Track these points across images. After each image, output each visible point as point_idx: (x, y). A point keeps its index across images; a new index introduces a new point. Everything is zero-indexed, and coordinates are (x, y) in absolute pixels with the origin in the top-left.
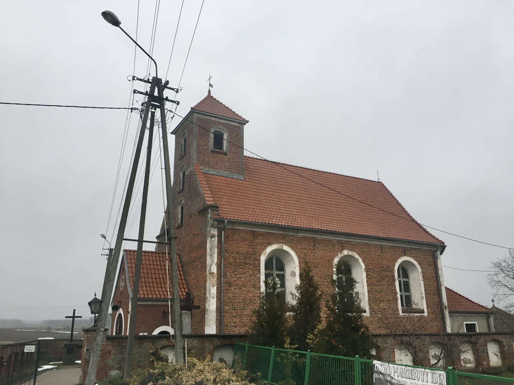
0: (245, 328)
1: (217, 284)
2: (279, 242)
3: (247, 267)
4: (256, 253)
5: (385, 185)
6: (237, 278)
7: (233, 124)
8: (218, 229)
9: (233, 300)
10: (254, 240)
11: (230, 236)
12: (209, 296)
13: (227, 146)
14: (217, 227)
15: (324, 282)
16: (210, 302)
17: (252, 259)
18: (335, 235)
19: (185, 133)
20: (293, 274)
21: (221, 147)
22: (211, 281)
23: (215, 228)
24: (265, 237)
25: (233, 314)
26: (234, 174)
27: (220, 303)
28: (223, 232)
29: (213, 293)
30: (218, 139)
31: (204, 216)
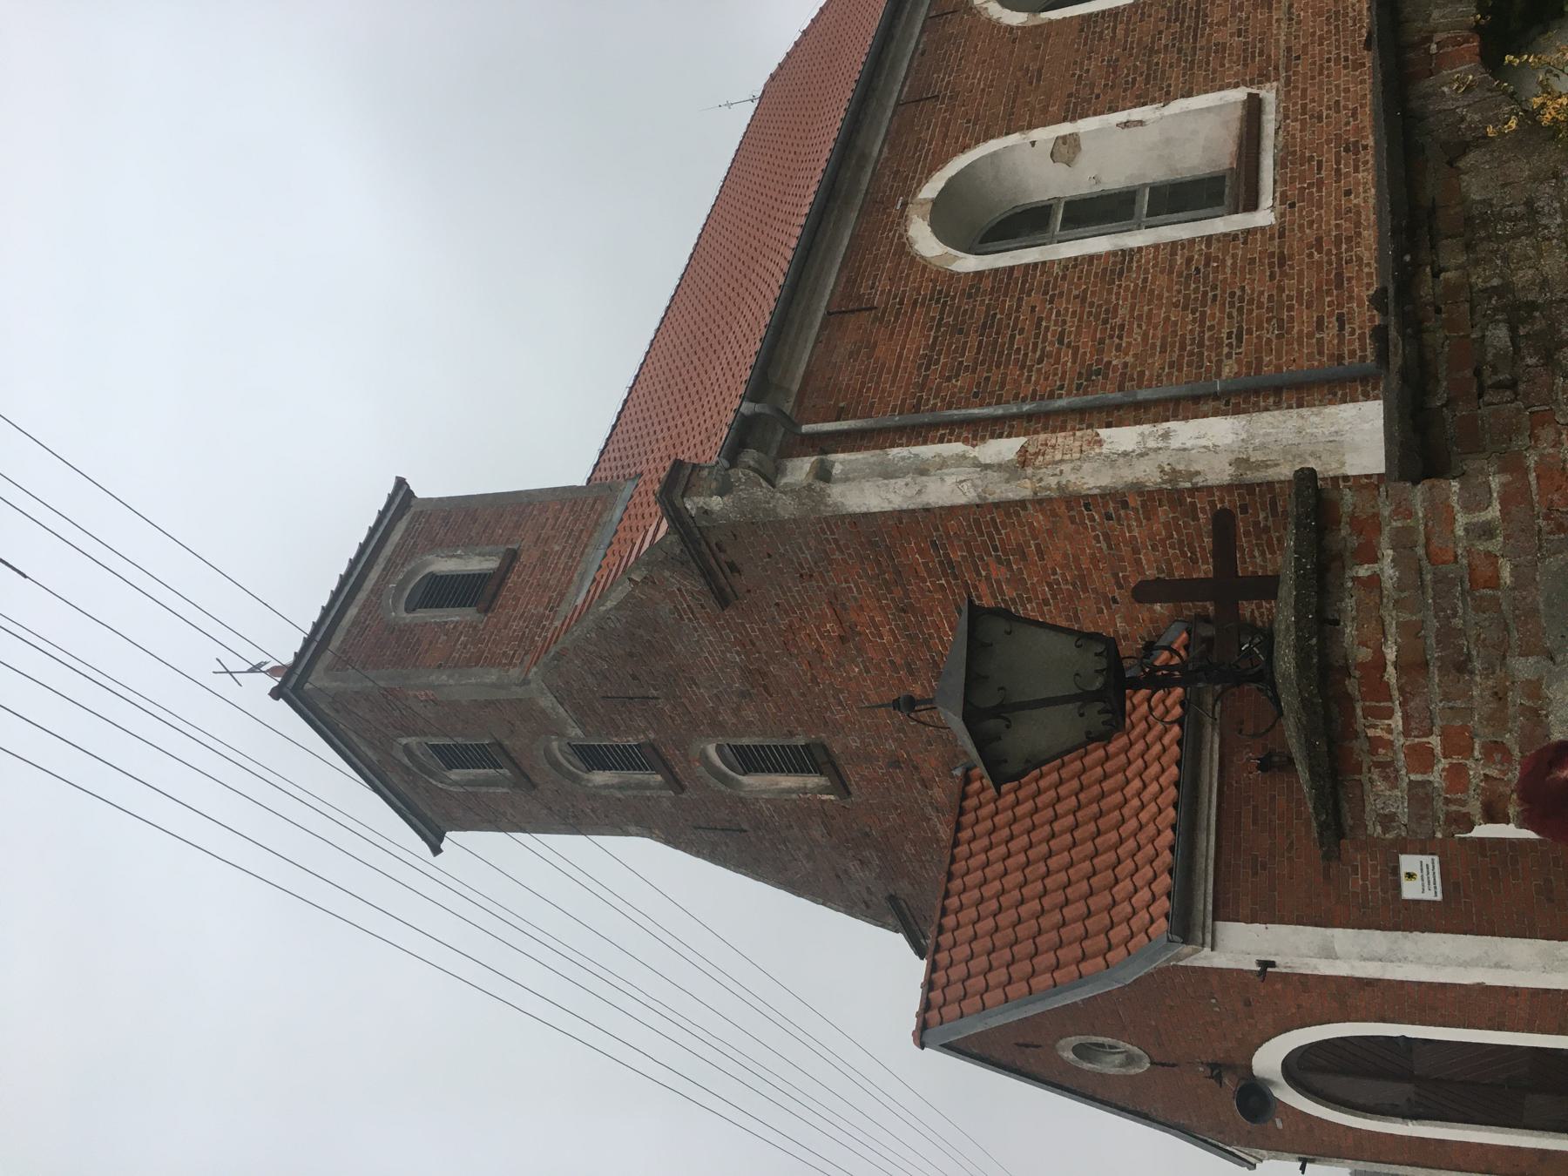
0: (1349, 279)
2: (901, 217)
5: (773, 68)
7: (396, 537)
8: (791, 456)
9: (1183, 348)
10: (872, 308)
12: (1152, 455)
13: (479, 555)
15: (1113, 38)
16: (1188, 445)
17: (967, 303)
19: (407, 748)
20: (1064, 149)
21: (479, 579)
22: (1067, 457)
24: (865, 271)
26: (605, 518)
27: (1196, 399)
28: (805, 428)
29: (1140, 438)
30: (441, 591)
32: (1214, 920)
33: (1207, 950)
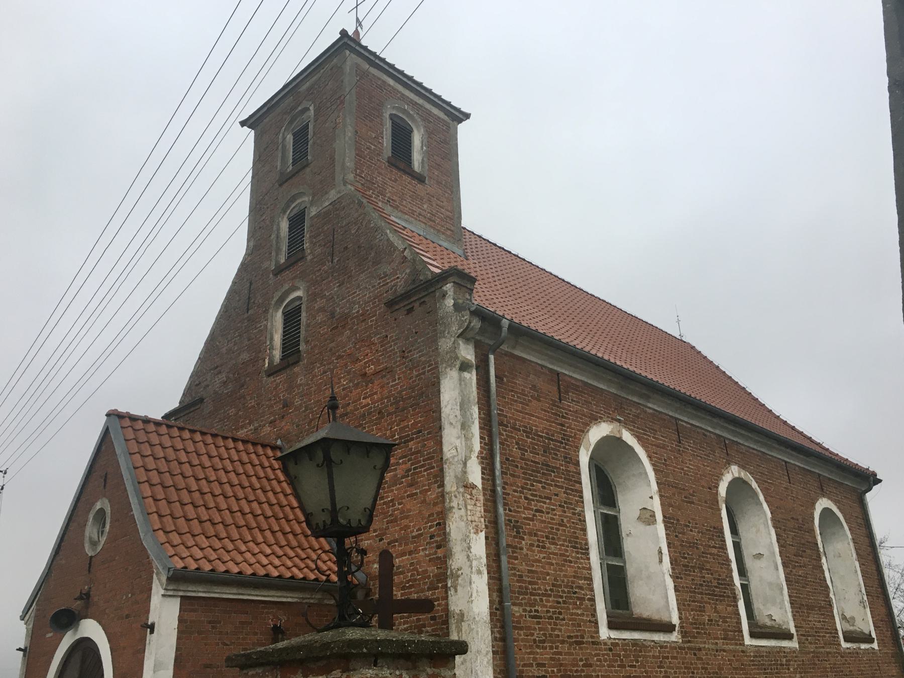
1: (485, 525)
3: (553, 480)
4: (568, 440)
5: (699, 348)
6: (532, 510)
7: (435, 111)
8: (476, 347)
9: (530, 583)
11: (505, 376)
14: (473, 340)
16: (474, 586)
18: (715, 420)
20: (648, 516)
23: (467, 340)
24: (582, 396)
25: (532, 635)
31: (418, 310)
32: (182, 597)
33: (162, 592)
